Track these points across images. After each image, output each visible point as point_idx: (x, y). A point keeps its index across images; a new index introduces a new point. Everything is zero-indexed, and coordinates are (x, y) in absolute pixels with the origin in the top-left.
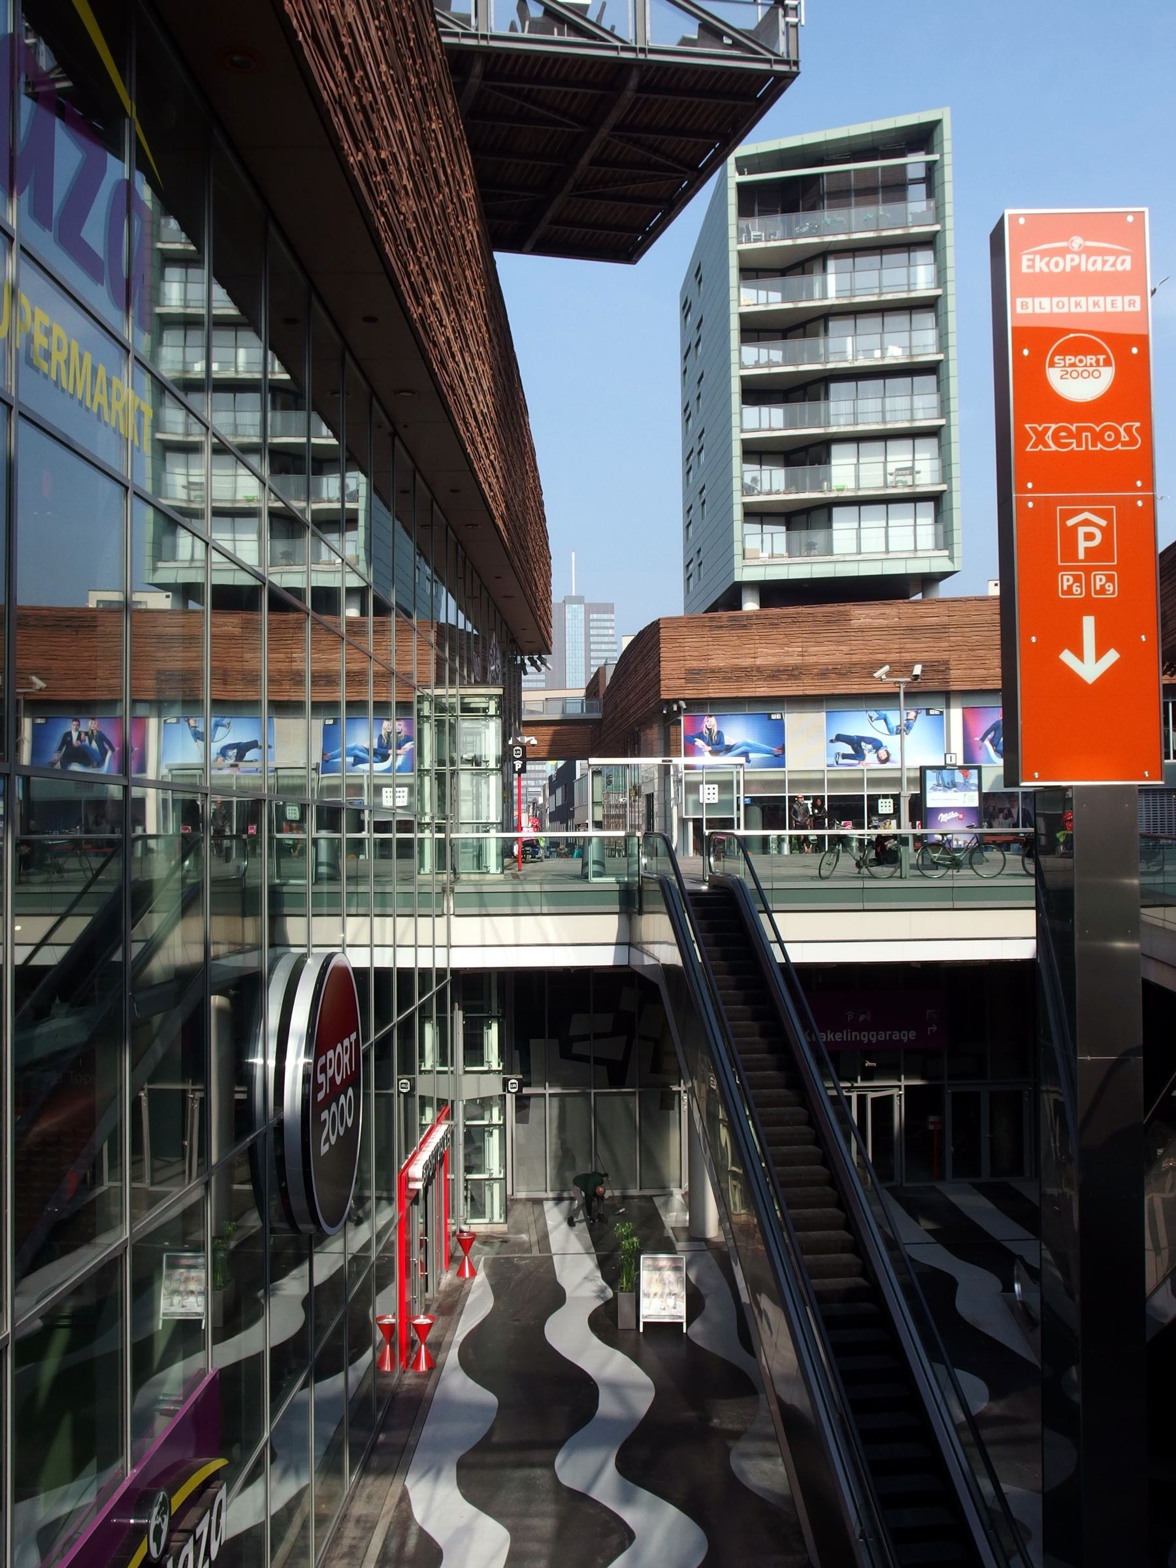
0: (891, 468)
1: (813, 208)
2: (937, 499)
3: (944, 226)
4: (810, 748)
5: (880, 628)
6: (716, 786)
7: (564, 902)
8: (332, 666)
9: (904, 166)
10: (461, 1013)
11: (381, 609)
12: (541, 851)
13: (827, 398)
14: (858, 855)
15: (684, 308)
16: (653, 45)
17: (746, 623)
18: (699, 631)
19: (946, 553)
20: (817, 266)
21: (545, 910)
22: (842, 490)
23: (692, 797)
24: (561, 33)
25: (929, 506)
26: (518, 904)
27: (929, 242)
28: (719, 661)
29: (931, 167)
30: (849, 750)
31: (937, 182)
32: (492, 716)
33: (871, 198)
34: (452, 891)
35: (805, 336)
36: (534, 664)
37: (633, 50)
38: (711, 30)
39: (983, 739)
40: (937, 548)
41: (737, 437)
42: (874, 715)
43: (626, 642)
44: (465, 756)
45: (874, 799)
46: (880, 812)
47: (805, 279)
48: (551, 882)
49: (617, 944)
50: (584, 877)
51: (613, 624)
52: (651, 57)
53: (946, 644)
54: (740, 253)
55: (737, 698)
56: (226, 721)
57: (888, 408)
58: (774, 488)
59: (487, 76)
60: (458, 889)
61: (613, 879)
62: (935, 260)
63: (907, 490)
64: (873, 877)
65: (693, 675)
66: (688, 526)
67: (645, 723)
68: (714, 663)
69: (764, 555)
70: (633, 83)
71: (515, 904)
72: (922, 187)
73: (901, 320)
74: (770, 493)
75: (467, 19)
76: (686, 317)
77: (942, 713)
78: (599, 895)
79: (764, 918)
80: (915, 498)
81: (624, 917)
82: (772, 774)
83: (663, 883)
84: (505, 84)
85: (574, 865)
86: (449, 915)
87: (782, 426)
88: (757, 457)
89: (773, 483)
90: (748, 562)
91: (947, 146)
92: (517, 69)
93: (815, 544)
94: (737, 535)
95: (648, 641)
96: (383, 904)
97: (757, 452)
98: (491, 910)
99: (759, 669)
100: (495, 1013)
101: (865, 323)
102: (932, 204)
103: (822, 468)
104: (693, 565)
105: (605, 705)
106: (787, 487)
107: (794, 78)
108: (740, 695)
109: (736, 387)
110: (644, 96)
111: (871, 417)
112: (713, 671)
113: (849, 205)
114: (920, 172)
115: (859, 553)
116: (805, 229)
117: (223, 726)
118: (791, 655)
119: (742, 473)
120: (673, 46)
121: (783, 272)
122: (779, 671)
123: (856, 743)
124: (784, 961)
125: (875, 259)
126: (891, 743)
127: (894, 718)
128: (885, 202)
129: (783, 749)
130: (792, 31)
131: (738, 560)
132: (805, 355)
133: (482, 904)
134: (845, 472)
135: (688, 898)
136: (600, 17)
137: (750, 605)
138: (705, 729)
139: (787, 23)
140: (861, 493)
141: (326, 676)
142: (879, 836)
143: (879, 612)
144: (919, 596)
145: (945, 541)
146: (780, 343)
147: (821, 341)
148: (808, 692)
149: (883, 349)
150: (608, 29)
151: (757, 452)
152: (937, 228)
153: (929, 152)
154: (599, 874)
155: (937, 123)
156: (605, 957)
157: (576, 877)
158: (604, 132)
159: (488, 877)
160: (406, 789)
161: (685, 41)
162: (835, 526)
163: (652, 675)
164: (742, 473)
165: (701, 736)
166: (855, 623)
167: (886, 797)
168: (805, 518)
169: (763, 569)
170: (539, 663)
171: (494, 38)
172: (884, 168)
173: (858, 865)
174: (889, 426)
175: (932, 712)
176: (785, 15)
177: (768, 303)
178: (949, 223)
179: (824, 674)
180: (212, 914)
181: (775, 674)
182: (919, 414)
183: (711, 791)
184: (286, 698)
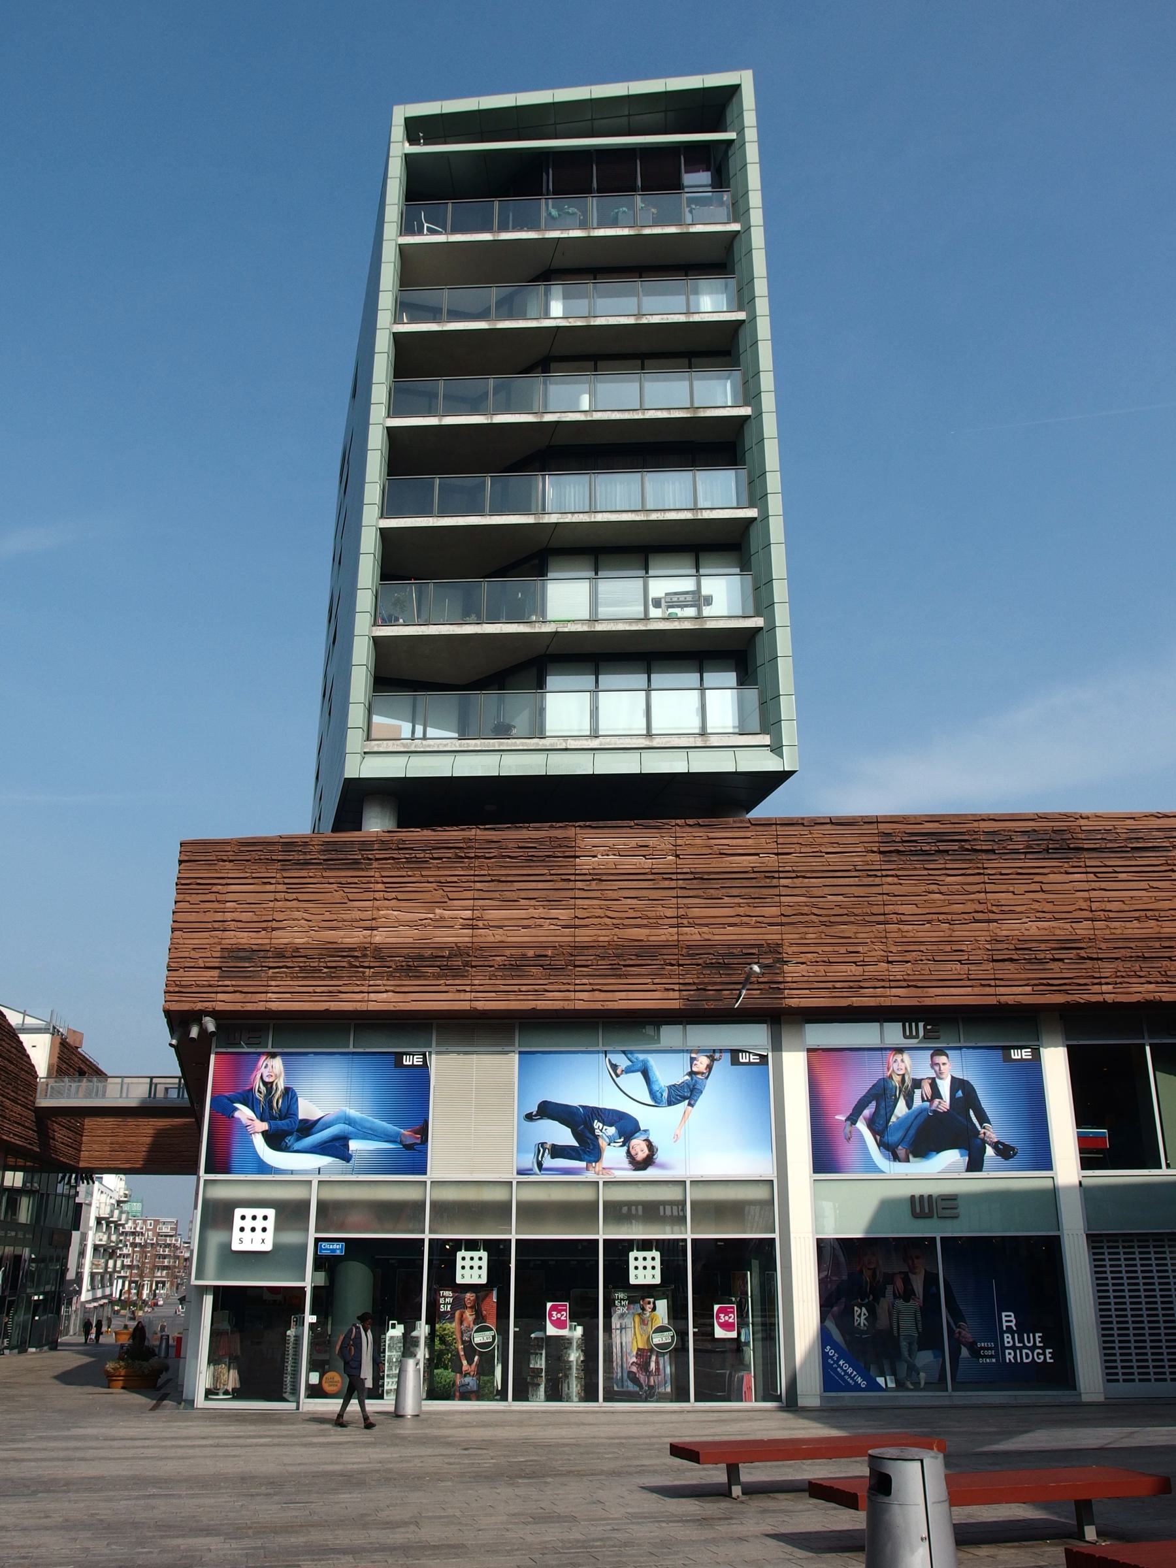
6: (271, 1213)
19: (766, 739)
28: (297, 931)
30: (564, 1136)
39: (853, 1119)
42: (622, 1061)
45: (619, 1251)
46: (633, 1281)
53: (774, 911)
68: (282, 938)
82: (397, 1188)
90: (374, 746)
91: (750, 118)
99: (379, 953)
112: (280, 954)
118: (448, 923)
122: (421, 958)
123: (581, 1121)
126: (659, 1123)
127: (669, 1071)
129: (423, 1131)
138: (258, 1084)
143: (633, 842)
148: (480, 1005)
165: (248, 1100)
166: (585, 863)
167: (645, 1245)
175: (743, 1058)
179: (516, 966)
181: (413, 964)
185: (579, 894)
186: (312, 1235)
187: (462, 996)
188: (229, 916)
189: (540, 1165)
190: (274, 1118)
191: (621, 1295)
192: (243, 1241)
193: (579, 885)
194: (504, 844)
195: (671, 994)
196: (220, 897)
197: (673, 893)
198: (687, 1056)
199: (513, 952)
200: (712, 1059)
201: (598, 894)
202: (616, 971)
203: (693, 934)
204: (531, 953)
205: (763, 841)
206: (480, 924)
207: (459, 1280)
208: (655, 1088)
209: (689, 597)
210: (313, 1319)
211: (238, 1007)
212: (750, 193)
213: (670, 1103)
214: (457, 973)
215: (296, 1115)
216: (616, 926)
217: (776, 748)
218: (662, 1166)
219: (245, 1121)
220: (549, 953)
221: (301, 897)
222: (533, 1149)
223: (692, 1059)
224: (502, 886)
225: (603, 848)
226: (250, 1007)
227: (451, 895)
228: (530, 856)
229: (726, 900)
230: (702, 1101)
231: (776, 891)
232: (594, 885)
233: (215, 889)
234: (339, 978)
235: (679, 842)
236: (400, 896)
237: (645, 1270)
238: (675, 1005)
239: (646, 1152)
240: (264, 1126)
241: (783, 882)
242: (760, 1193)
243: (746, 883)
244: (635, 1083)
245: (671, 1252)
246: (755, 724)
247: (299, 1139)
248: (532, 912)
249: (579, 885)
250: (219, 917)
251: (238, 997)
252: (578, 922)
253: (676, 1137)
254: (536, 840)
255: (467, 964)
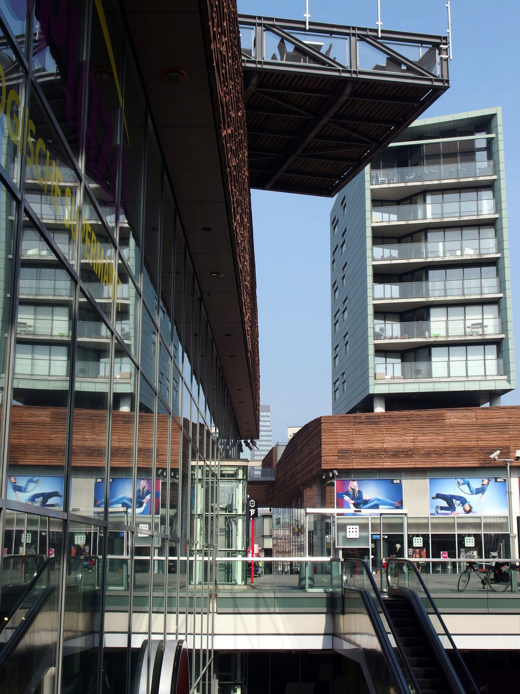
0: (469, 323)
1: (417, 164)
2: (499, 344)
3: (499, 176)
4: (419, 503)
5: (464, 425)
6: (358, 527)
7: (290, 606)
8: (102, 443)
9: (473, 140)
10: (217, 681)
11: (145, 409)
12: (260, 570)
13: (427, 279)
14: (483, 576)
15: (333, 223)
16: (360, 69)
17: (377, 420)
18: (347, 425)
19: (505, 377)
20: (420, 199)
21: (277, 610)
22: (438, 337)
23: (341, 534)
24: (305, 61)
25: (494, 347)
26: (259, 606)
27: (490, 186)
28: (360, 444)
29: (490, 141)
30: (444, 504)
31: (494, 150)
32: (240, 480)
33: (453, 159)
34: (216, 596)
35: (412, 241)
36: (247, 445)
37: (349, 72)
38: (395, 61)
40: (499, 374)
41: (371, 303)
42: (461, 481)
43: (292, 431)
44: (221, 506)
45: (462, 537)
46: (466, 546)
47: (412, 207)
48: (280, 591)
49: (324, 634)
50: (302, 588)
51: (269, 419)
52: (360, 76)
53: (507, 436)
54: (372, 190)
55: (371, 469)
56: (35, 479)
57: (465, 286)
58: (395, 335)
59: (260, 85)
60: (219, 595)
61: (321, 590)
62: (494, 197)
63: (479, 338)
64: (493, 591)
65: (343, 454)
66: (335, 358)
67: (308, 484)
68: (356, 446)
69: (388, 377)
70: (348, 91)
71: (257, 606)
72: (485, 153)
73: (472, 233)
74: (391, 338)
75: (249, 52)
76: (334, 228)
77: (505, 480)
78: (313, 600)
79: (433, 619)
80: (484, 343)
81: (330, 616)
83: (363, 594)
84: (268, 90)
85: (294, 579)
86: (213, 613)
87: (398, 297)
88: (383, 315)
89: (393, 332)
90: (377, 381)
91: (500, 129)
92: (305, 83)
93: (420, 371)
94: (371, 364)
95: (311, 433)
96: (170, 605)
97: (383, 312)
98: (242, 610)
99: (385, 450)
100: (239, 681)
101: (451, 234)
102: (491, 163)
103: (425, 322)
104: (338, 382)
105: (277, 472)
106: (402, 334)
107: (445, 90)
108: (373, 467)
109: (370, 272)
110: (352, 98)
111: (455, 292)
112: (355, 451)
113: (439, 163)
114: (484, 144)
115: (449, 376)
116: (412, 177)
117: (33, 482)
118: (406, 441)
119: (374, 325)
120: (370, 70)
121: (398, 202)
122: (399, 452)
123: (449, 499)
124: (451, 647)
125: (456, 196)
126: (472, 499)
127: (476, 483)
128: (461, 161)
130: (444, 63)
131: (371, 380)
132: (413, 253)
133: (236, 606)
134: (438, 326)
135: (383, 603)
136: (328, 51)
137: (379, 409)
138: (350, 489)
139: (441, 58)
140: (449, 339)
141: (98, 450)
142: (497, 563)
144: (487, 405)
145: (504, 369)
146: (397, 245)
147: (423, 245)
148: (418, 466)
149: (462, 250)
150: (332, 58)
151: (383, 312)
152: (495, 177)
153: (488, 133)
154: (311, 586)
155: (495, 115)
156: (316, 643)
157: (294, 588)
158: (326, 119)
159: (236, 587)
160: (147, 526)
161: (377, 67)
162: (433, 359)
163: (314, 453)
164: (374, 325)
165: (347, 494)
166: (448, 422)
167: (469, 535)
168: (413, 354)
169: (387, 386)
170: (251, 444)
171: (266, 63)
172: (461, 141)
173: (483, 582)
174: (467, 298)
175: (499, 480)
176: (440, 54)
177: (389, 221)
178: (502, 174)
179: (428, 454)
180: (66, 610)
181: (396, 454)
182: (485, 291)
183: (354, 530)
184: (81, 465)
185: (446, 431)
186: (370, 533)
187: (412, 463)
188: (338, 440)
189: (437, 512)
190: (356, 499)
191: (463, 550)
192: (350, 535)
193: (446, 428)
194: (422, 416)
195: (476, 462)
196: (335, 434)
197: (476, 431)
198: (481, 480)
199: (427, 449)
200: (489, 480)
201: (452, 431)
202: (458, 455)
203: (482, 443)
204: (432, 450)
205: (503, 413)
206: (416, 441)
207: (414, 546)
208: (471, 489)
209: (479, 326)
210: (373, 557)
211: (344, 467)
212: (498, 127)
213: (476, 494)
214: (410, 456)
215: (362, 498)
216: (458, 441)
217: (509, 381)
218: (474, 512)
219: (347, 500)
220: (438, 450)
221: (360, 433)
222: (435, 508)
223: (483, 481)
224: (422, 429)
225: (453, 416)
226: (348, 467)
227: (407, 432)
228: (431, 420)
229: (492, 433)
230: (486, 493)
231: (508, 430)
232: (451, 428)
233: (333, 431)
234: (374, 458)
235: (477, 414)
236: (391, 433)
237: (470, 542)
238: (477, 465)
239: (469, 508)
240: (353, 502)
241: (510, 427)
242: (504, 521)
243: (498, 427)
244: (465, 488)
245: (477, 537)
246: (502, 373)
247: (364, 505)
248: (433, 437)
249: (446, 428)
250: (336, 440)
251: (344, 464)
252: (446, 440)
253: (478, 504)
254: (431, 414)
255: (413, 453)
